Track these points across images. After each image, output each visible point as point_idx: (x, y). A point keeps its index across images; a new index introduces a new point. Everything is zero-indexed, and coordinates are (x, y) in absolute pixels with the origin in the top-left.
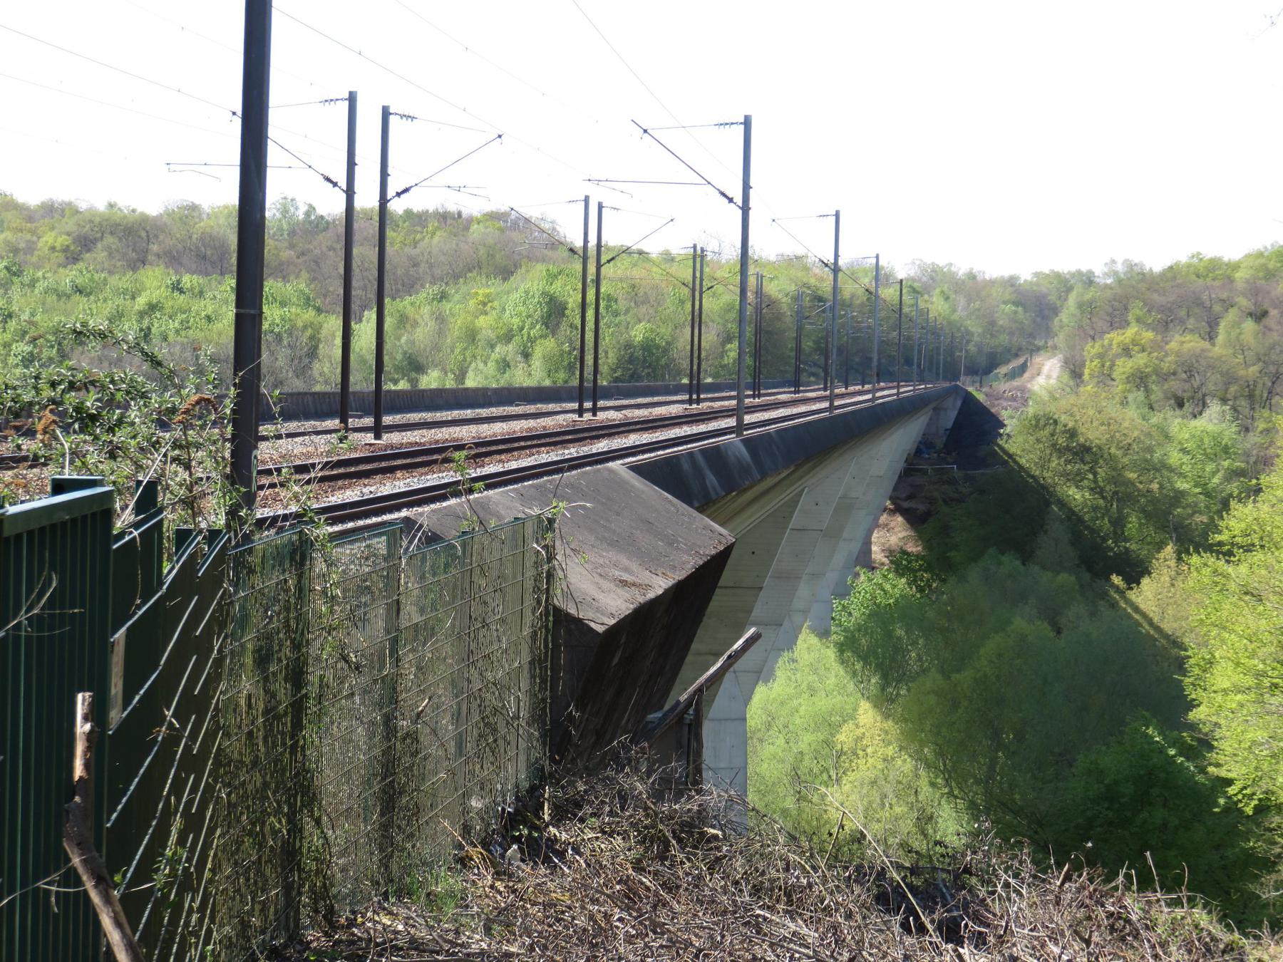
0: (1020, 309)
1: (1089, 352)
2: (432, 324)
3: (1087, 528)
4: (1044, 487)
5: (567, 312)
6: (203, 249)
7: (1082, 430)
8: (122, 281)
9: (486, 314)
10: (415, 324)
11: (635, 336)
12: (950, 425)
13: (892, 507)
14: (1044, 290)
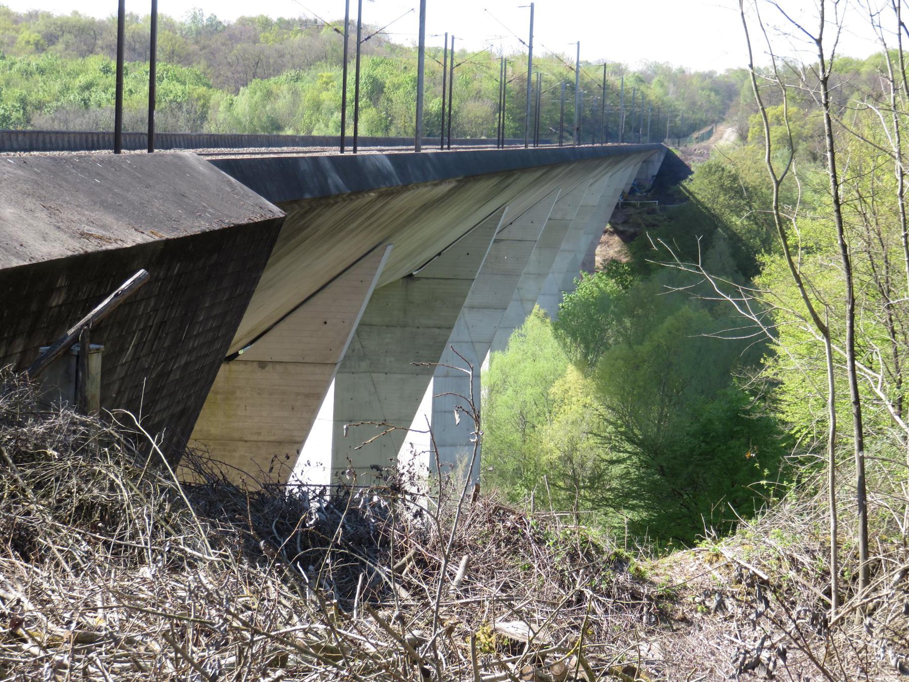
0: (713, 94)
1: (752, 121)
2: (288, 97)
3: (745, 245)
4: (713, 215)
5: (385, 90)
6: (133, 43)
7: (742, 175)
8: (72, 65)
9: (328, 90)
10: (277, 97)
11: (433, 107)
12: (655, 173)
13: (612, 230)
14: (733, 81)
